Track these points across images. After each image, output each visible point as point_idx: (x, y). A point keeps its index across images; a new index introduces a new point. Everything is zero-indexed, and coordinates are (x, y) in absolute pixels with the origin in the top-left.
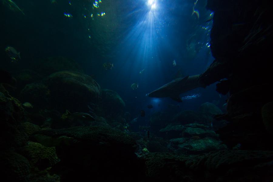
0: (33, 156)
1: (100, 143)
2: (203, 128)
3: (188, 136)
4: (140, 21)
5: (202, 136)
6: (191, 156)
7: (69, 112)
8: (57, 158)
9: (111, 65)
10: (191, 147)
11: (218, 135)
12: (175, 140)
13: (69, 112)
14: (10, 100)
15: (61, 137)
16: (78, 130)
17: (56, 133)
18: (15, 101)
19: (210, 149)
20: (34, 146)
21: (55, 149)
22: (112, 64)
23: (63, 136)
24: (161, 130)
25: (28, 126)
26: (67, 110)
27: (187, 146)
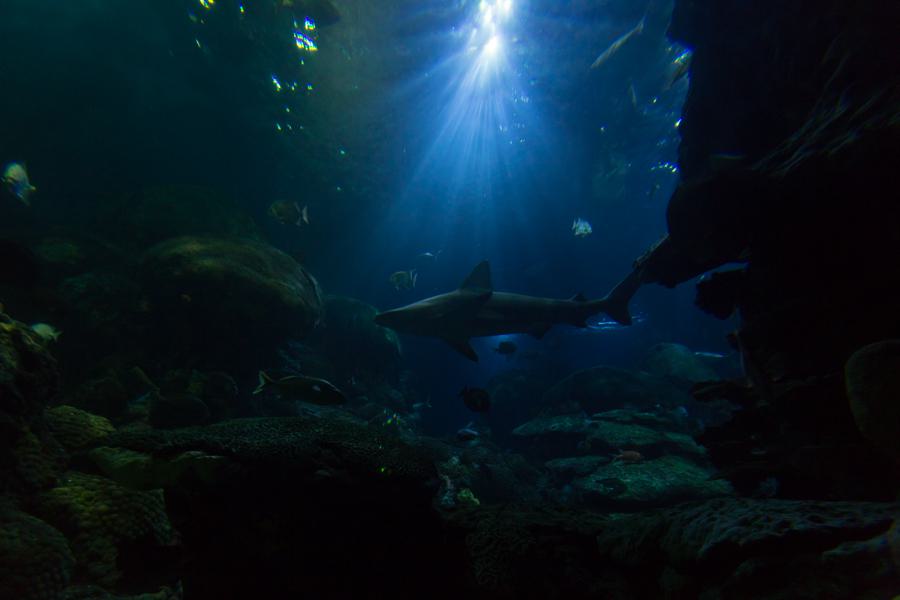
0: (85, 523)
1: (320, 472)
2: (650, 424)
3: (605, 450)
4: (462, 75)
5: (652, 452)
6: (614, 517)
7: (268, 378)
8: (168, 527)
9: (299, 210)
10: (622, 488)
11: (702, 449)
12: (563, 463)
13: (268, 378)
14: (5, 331)
15: (184, 456)
16: (245, 430)
17: (170, 443)
18: (24, 333)
19: (683, 496)
20: (87, 489)
21: (162, 499)
22: (301, 209)
23: (192, 453)
24: (518, 430)
25: (68, 421)
26: (261, 373)
27: (606, 482)
